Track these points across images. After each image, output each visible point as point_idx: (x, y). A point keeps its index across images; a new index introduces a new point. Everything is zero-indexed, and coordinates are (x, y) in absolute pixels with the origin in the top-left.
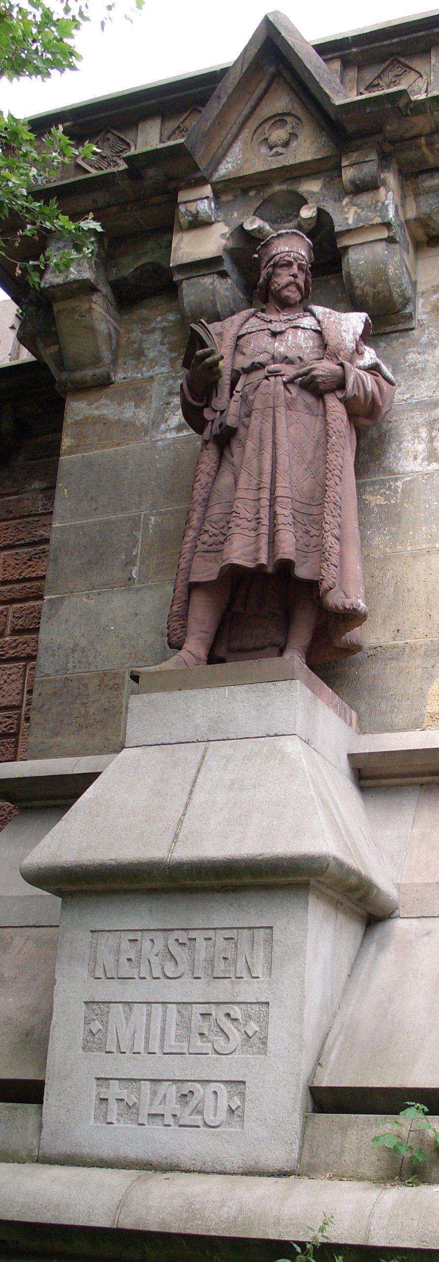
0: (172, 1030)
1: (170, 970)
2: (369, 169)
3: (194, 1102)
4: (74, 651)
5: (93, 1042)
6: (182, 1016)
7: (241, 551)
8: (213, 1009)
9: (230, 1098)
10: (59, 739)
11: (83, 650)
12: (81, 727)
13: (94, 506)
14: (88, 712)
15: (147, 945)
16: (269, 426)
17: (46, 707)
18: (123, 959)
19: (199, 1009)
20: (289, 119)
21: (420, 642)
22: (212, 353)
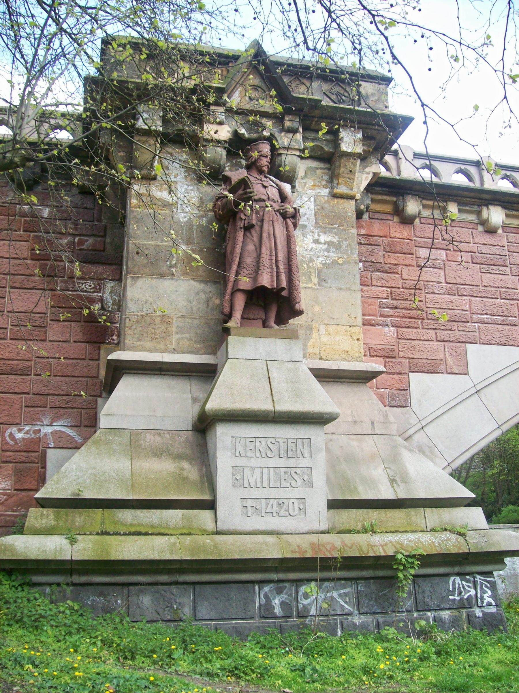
0: (272, 479)
1: (269, 453)
2: (296, 125)
3: (285, 507)
4: (146, 303)
5: (238, 483)
6: (276, 472)
7: (266, 280)
8: (289, 470)
9: (299, 504)
10: (142, 343)
11: (151, 303)
12: (152, 339)
13: (151, 236)
14: (156, 333)
15: (258, 444)
16: (271, 228)
17: (133, 327)
18: (248, 449)
19: (283, 470)
20: (259, 89)
21: (304, 323)
22: (251, 193)
